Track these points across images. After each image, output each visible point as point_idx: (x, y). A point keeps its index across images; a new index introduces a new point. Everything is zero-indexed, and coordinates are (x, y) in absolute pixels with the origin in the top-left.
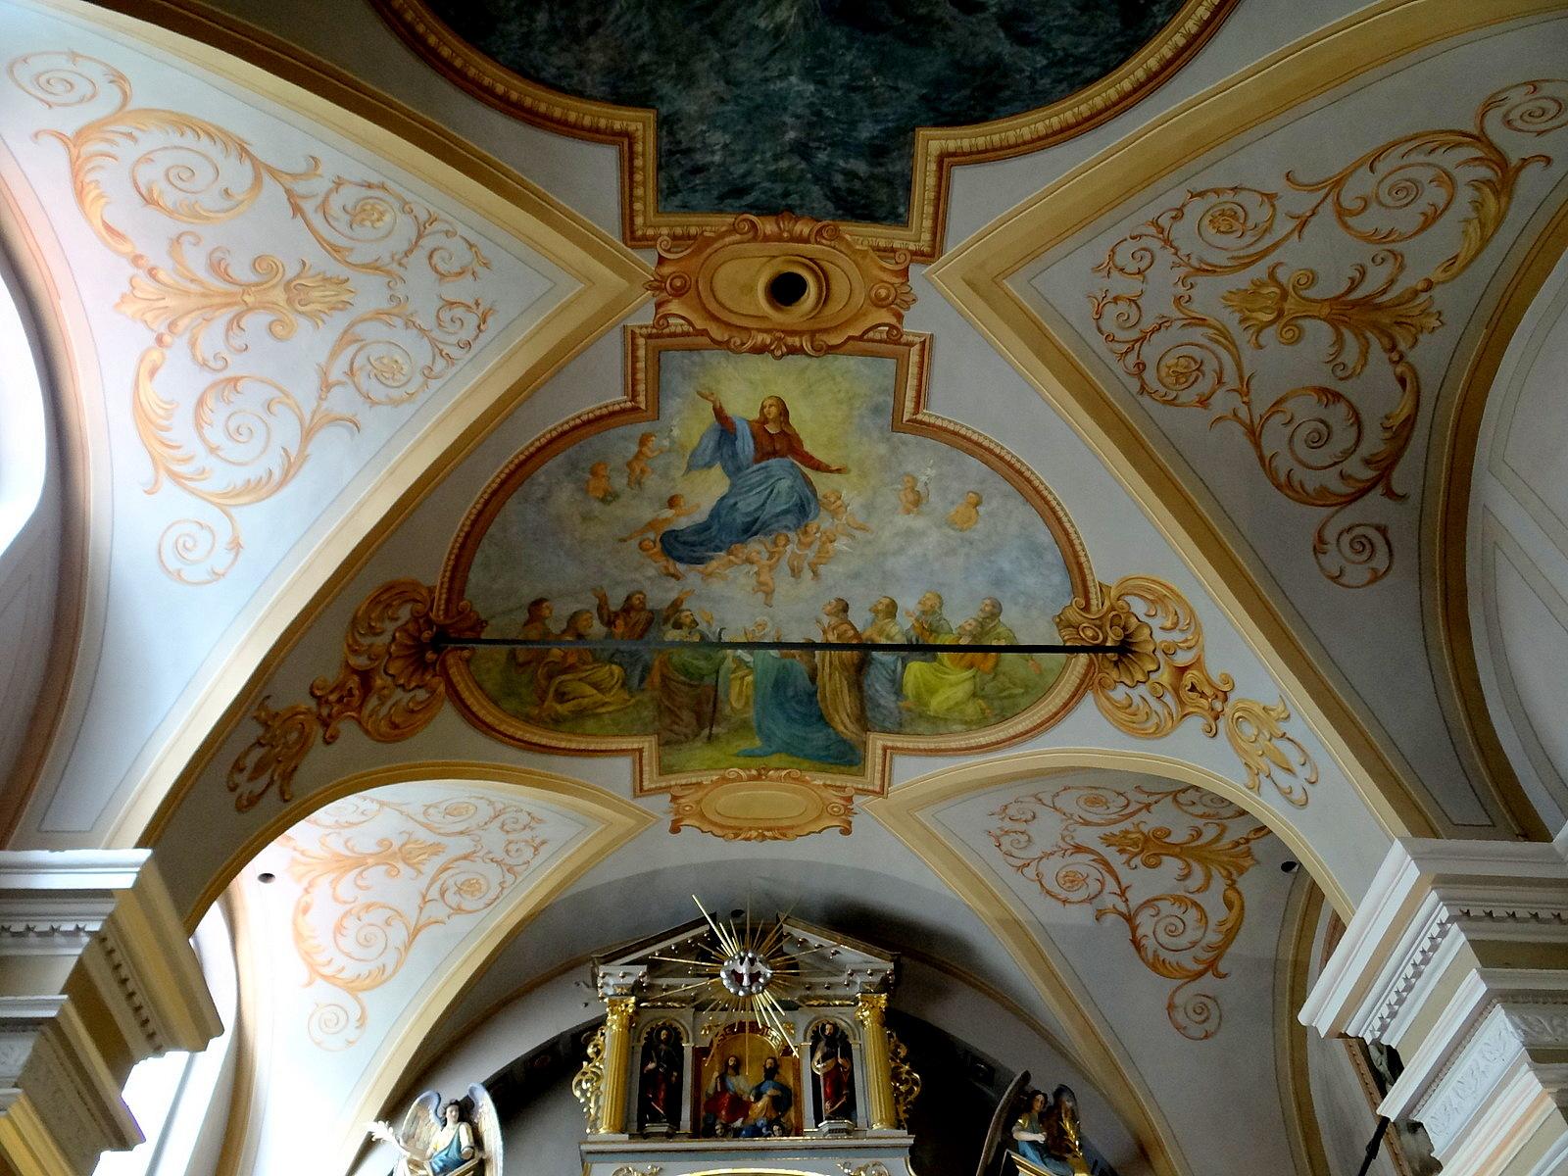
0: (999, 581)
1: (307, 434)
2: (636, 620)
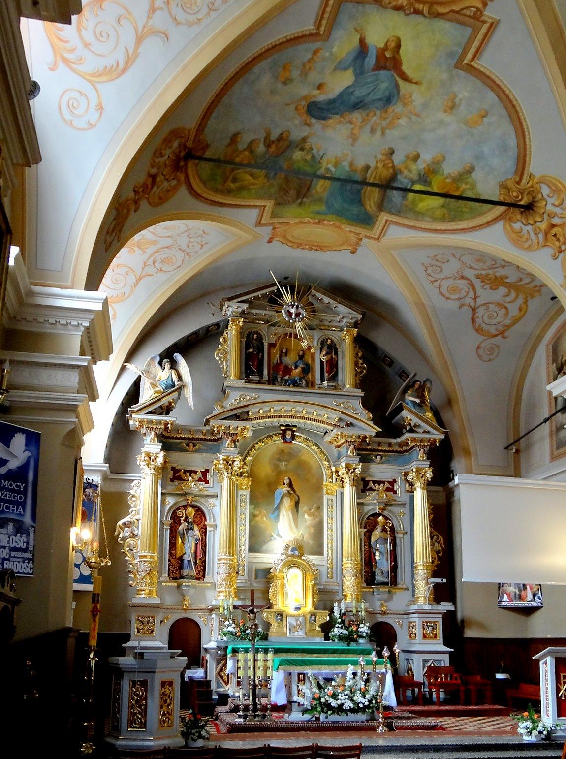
0: (479, 157)
1: (139, 40)
2: (282, 145)
